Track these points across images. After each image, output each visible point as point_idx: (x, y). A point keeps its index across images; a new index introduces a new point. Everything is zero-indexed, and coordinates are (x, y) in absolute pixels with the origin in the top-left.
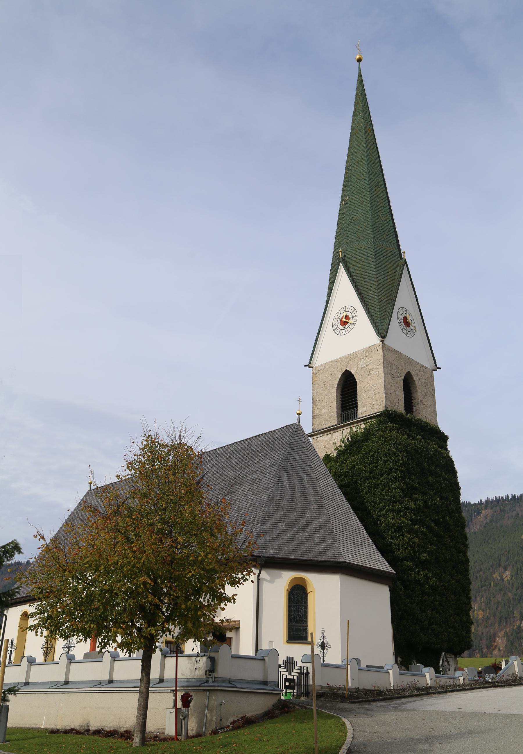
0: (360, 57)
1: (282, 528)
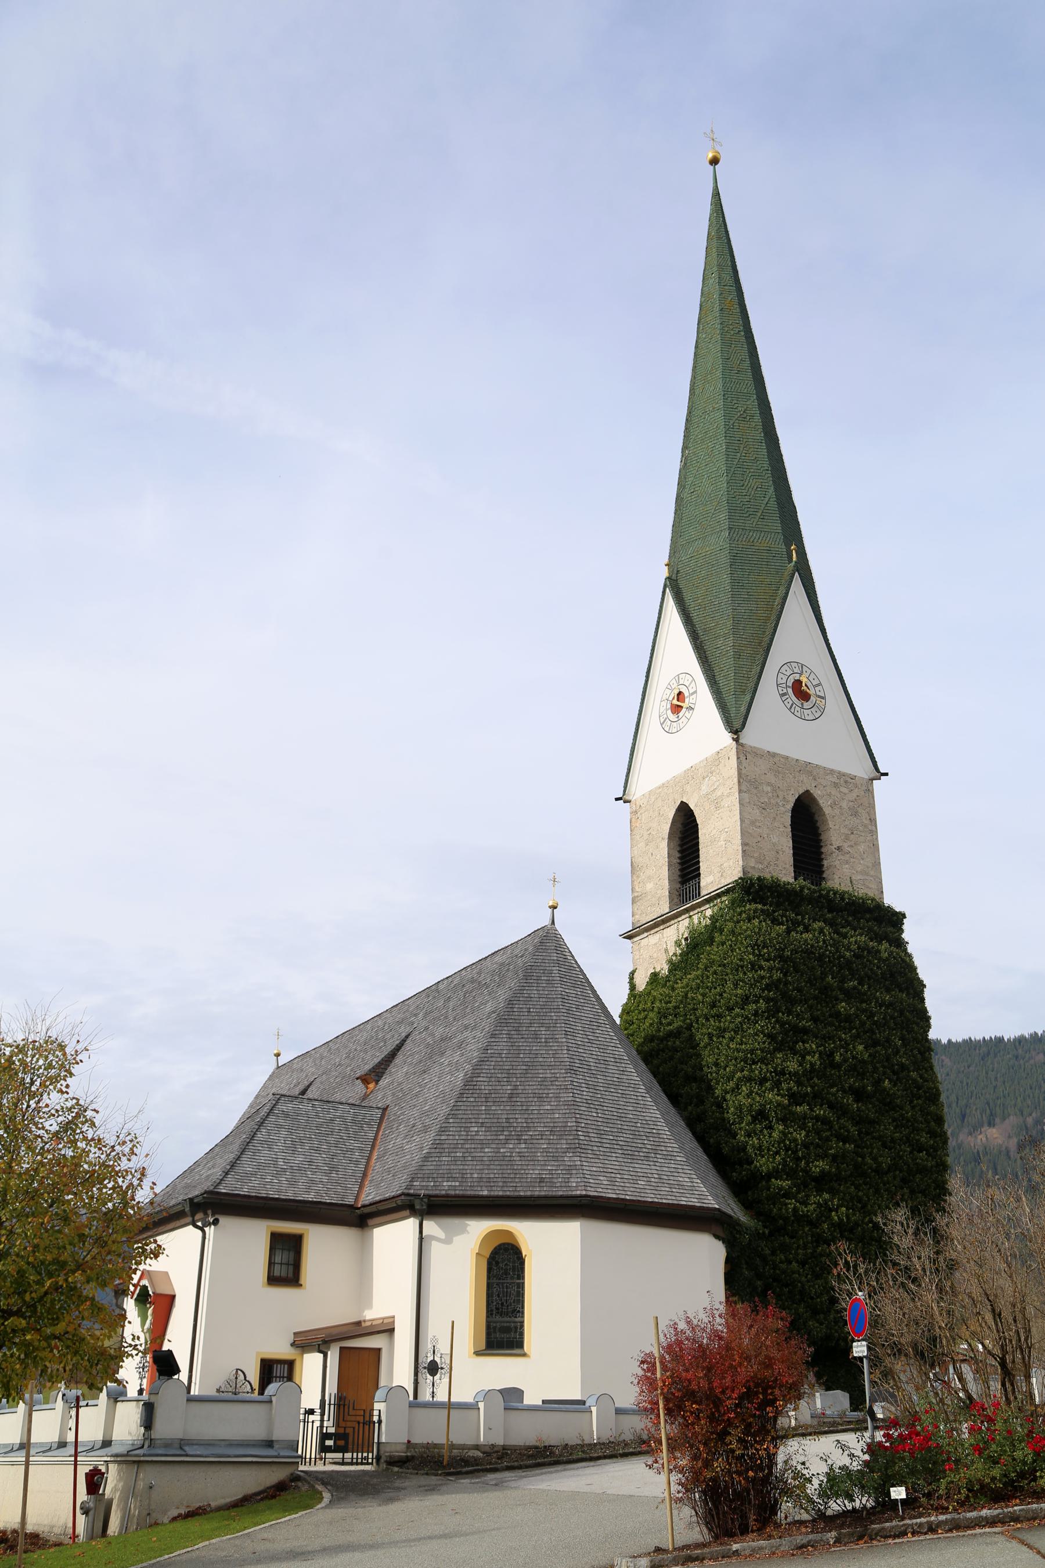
0: (714, 154)
1: (476, 1137)
